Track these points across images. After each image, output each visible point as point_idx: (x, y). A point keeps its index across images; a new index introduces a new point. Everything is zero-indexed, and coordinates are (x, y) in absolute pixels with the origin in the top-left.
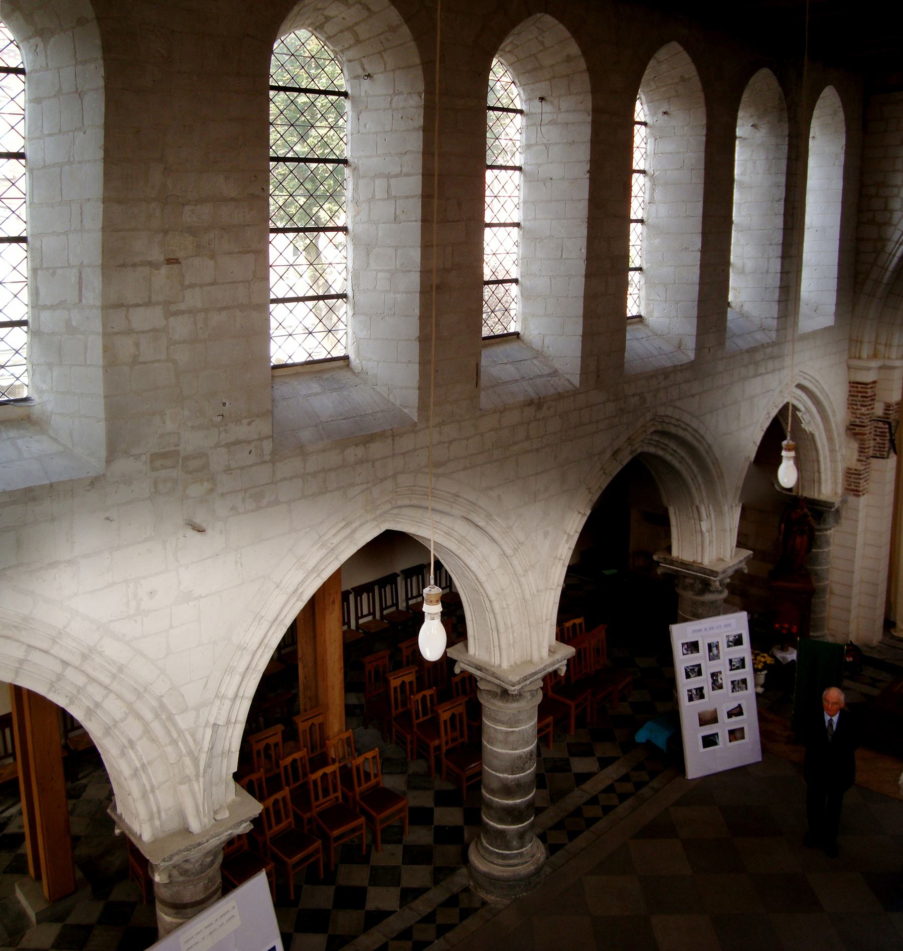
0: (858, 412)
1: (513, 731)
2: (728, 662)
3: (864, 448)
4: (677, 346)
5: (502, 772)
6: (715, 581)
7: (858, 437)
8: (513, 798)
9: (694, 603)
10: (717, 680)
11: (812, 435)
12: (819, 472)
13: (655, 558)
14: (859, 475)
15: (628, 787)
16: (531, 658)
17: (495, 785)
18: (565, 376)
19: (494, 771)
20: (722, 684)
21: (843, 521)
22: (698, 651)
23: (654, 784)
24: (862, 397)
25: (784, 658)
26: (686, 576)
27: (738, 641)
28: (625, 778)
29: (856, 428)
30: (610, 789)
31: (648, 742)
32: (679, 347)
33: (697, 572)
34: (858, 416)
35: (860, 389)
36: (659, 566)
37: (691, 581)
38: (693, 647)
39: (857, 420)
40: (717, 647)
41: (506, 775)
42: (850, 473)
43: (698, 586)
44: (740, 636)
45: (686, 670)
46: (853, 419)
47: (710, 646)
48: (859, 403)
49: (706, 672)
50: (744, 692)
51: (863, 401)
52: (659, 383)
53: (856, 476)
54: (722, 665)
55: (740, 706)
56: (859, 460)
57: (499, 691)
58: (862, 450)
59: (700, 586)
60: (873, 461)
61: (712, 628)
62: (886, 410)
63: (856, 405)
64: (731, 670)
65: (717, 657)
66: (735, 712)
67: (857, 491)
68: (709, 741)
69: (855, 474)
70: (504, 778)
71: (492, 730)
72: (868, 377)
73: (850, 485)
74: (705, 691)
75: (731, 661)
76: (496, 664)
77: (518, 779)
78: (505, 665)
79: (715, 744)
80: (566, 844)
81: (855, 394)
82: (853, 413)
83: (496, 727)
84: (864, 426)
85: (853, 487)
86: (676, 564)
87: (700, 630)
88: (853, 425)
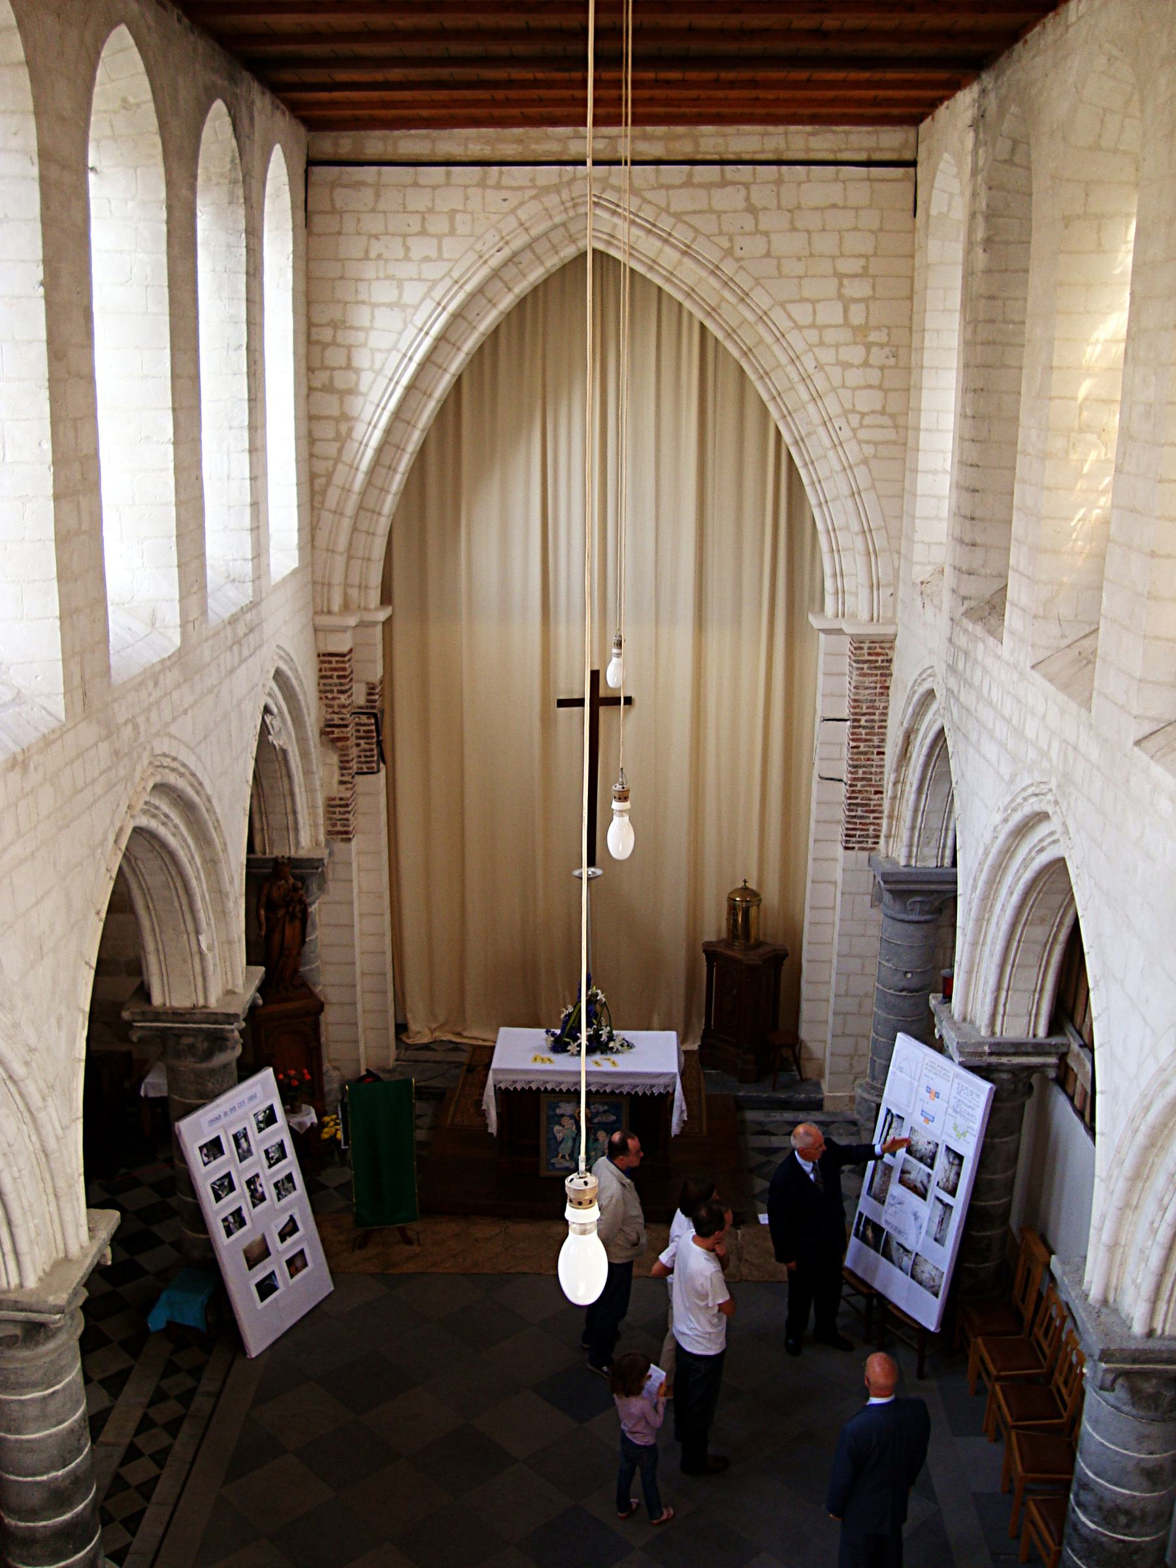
0: (336, 702)
1: (54, 1393)
2: (263, 1155)
3: (348, 762)
4: (149, 623)
5: (47, 1472)
6: (232, 1031)
7: (339, 744)
8: (71, 1507)
9: (199, 1075)
10: (256, 1189)
11: (284, 752)
12: (295, 813)
13: (126, 1015)
14: (347, 806)
15: (171, 1408)
16: (66, 1251)
17: (35, 1499)
18: (37, 699)
19: (31, 1476)
20: (263, 1194)
21: (330, 885)
22: (222, 1153)
23: (208, 1385)
24: (339, 677)
25: (300, 1124)
26: (179, 1034)
27: (270, 1118)
28: (159, 1397)
29: (336, 730)
30: (145, 1424)
31: (170, 1324)
32: (153, 625)
33: (201, 1023)
34: (336, 710)
35: (334, 665)
36: (132, 1027)
37: (190, 1040)
38: (214, 1148)
39: (335, 716)
40: (245, 1136)
41: (53, 1474)
42: (332, 806)
43: (202, 1046)
44: (271, 1108)
45: (213, 1188)
46: (329, 717)
47: (236, 1137)
48: (335, 689)
49: (240, 1182)
50: (294, 1194)
51: (341, 684)
52: (150, 695)
53: (342, 810)
54: (257, 1164)
55: (292, 1218)
56: (342, 783)
57: (18, 1331)
58: (344, 766)
59: (206, 1045)
60: (359, 779)
61: (233, 1109)
62: (369, 694)
63: (332, 691)
64: (270, 1166)
65: (249, 1152)
66: (287, 1229)
67: (346, 833)
68: (266, 1288)
69: (340, 806)
70: (50, 1481)
71: (15, 1407)
72: (341, 644)
73: (334, 825)
74: (245, 1213)
75: (267, 1152)
76: (13, 1285)
77: (74, 1471)
78: (31, 1283)
79: (275, 1288)
80: (130, 1544)
81: (328, 673)
82: (327, 706)
83: (23, 1398)
84: (346, 726)
85: (339, 828)
86: (164, 1017)
87: (218, 1118)
88: (330, 726)
